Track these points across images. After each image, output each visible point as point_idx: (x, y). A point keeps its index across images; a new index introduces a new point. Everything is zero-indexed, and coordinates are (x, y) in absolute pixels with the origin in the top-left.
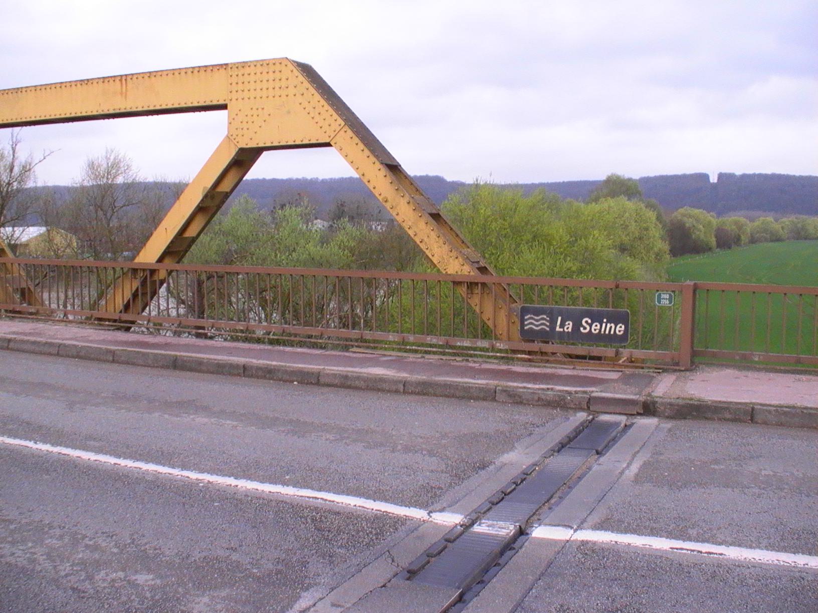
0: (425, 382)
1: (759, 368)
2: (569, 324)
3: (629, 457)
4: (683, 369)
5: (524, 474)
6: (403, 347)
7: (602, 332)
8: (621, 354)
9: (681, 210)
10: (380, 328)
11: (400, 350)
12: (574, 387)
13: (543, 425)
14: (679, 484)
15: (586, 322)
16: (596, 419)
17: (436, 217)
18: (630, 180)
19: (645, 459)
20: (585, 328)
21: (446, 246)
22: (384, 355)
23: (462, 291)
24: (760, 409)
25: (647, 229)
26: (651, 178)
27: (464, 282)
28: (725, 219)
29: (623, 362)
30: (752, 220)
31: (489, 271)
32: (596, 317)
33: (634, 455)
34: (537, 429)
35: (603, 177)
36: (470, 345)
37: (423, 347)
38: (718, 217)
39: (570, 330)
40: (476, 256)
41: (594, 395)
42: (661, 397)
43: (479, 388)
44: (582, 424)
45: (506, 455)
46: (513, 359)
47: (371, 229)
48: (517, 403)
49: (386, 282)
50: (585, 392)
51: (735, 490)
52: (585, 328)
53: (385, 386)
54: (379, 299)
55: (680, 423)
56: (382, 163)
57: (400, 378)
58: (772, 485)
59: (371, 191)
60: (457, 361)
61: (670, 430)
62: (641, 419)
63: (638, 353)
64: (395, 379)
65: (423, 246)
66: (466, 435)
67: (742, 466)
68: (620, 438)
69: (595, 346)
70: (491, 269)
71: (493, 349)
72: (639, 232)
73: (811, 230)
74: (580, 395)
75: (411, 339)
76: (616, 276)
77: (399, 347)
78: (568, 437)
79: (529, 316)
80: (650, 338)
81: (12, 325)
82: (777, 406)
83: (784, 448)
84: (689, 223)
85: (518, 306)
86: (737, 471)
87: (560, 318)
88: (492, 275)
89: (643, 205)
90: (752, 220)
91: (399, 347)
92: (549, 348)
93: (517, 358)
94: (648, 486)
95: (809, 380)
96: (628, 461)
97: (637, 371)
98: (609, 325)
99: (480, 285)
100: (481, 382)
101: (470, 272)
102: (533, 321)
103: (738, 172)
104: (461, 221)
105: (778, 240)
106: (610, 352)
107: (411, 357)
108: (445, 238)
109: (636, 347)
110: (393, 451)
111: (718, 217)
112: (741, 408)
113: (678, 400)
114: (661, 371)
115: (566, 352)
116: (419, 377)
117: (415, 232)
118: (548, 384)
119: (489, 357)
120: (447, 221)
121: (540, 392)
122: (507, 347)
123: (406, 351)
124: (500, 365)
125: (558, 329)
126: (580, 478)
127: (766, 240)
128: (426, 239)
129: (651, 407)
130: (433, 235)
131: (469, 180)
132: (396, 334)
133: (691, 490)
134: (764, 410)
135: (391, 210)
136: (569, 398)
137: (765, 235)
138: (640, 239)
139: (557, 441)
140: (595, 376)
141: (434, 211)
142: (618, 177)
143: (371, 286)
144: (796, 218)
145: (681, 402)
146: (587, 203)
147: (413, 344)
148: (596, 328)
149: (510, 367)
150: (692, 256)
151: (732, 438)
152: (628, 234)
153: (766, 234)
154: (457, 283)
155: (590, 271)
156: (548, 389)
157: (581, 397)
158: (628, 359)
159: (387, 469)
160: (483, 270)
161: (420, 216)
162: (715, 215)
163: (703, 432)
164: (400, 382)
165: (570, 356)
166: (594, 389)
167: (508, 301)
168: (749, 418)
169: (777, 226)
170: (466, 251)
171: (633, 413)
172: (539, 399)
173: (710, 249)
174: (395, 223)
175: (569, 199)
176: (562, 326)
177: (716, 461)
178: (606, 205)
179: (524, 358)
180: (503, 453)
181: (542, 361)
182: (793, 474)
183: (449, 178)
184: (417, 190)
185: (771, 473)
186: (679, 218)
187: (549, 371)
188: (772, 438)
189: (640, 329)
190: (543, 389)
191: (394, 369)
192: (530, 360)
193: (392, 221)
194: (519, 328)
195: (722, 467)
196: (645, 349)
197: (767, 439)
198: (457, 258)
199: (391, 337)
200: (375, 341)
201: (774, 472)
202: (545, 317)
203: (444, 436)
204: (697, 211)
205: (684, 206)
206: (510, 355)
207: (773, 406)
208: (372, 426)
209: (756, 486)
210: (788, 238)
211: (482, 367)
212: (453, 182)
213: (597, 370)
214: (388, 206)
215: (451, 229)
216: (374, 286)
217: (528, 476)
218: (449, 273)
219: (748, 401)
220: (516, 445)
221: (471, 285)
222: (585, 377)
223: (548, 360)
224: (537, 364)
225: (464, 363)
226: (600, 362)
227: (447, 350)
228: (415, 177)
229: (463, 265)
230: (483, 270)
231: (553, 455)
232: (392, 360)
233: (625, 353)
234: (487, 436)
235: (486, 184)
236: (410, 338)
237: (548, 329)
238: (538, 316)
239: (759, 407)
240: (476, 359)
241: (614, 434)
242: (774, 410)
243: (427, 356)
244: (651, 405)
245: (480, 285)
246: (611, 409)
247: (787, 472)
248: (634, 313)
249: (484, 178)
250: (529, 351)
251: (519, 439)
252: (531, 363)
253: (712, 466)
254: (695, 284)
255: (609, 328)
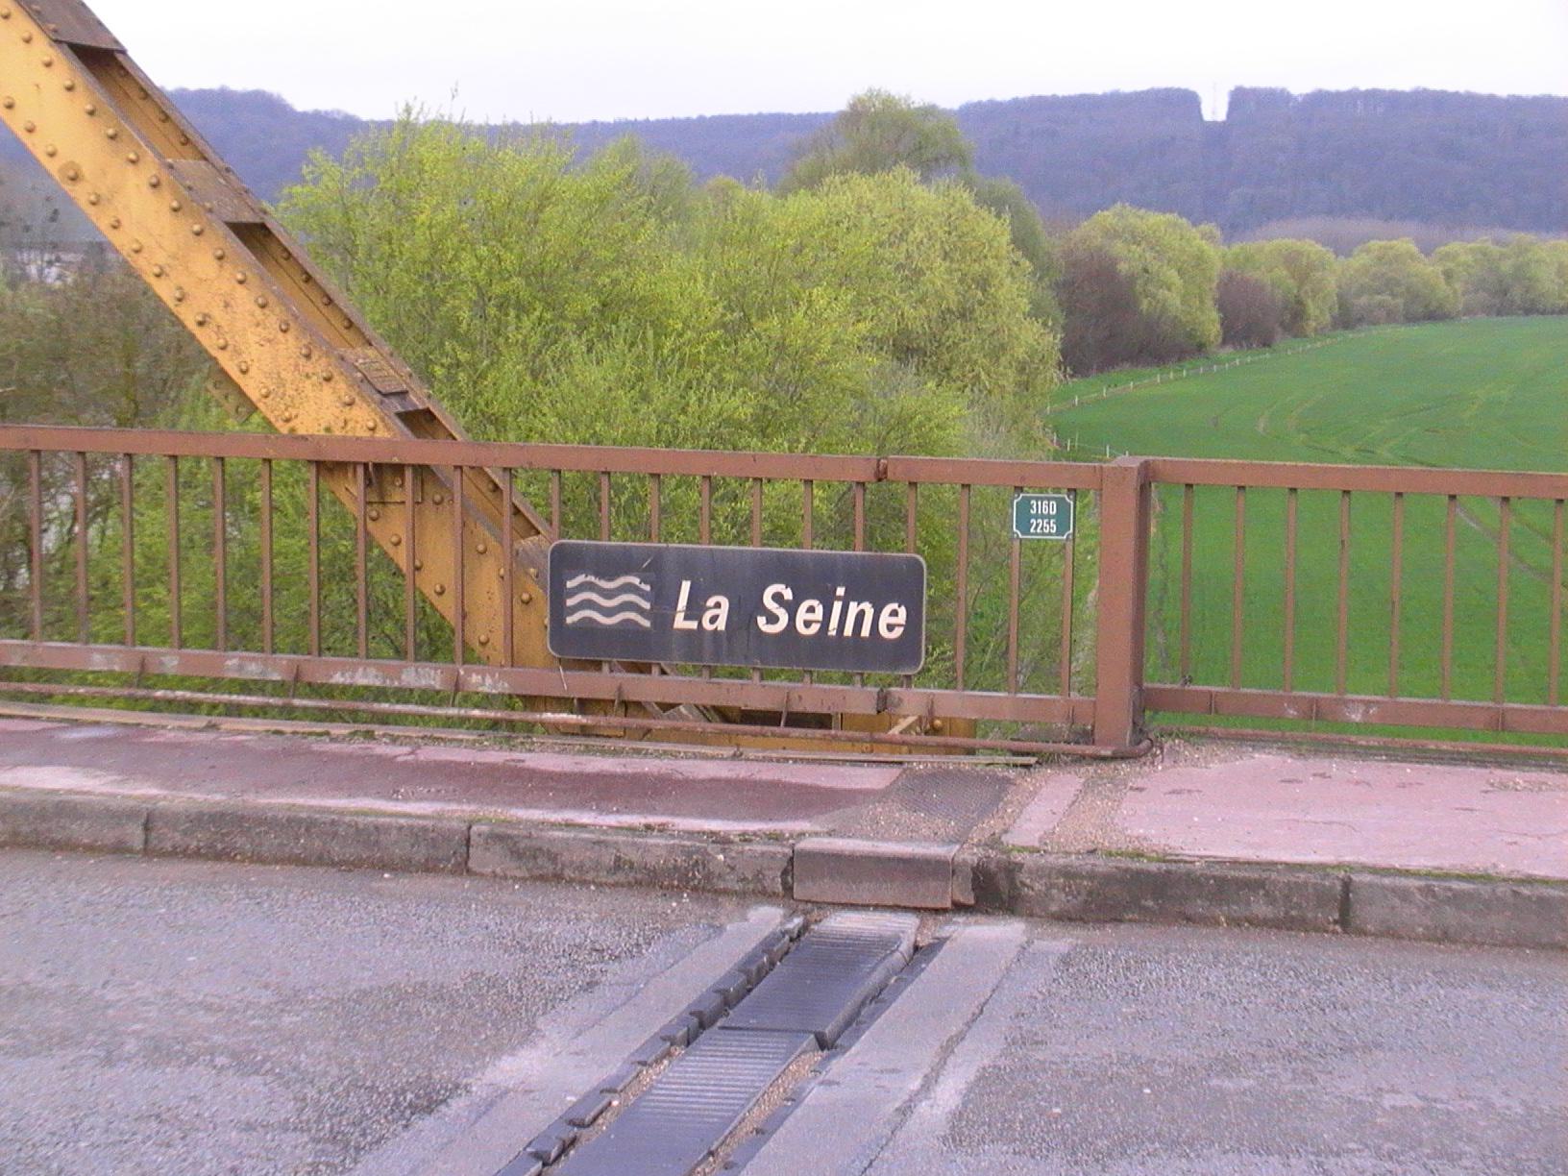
0: (223, 815)
1: (1368, 748)
2: (718, 605)
3: (927, 1057)
4: (1108, 753)
5: (572, 1123)
6: (141, 692)
7: (832, 632)
8: (898, 705)
9: (1107, 217)
10: (57, 627)
11: (133, 703)
12: (737, 819)
13: (634, 951)
14: (1103, 1144)
15: (778, 598)
16: (814, 927)
17: (254, 235)
18: (929, 111)
19: (986, 1062)
20: (773, 619)
21: (290, 336)
22: (76, 723)
23: (351, 491)
24: (1370, 885)
25: (984, 283)
26: (1000, 104)
27: (355, 464)
28: (1251, 246)
29: (904, 732)
30: (1342, 247)
31: (440, 423)
32: (812, 582)
33: (947, 1049)
34: (615, 966)
35: (833, 100)
36: (378, 683)
37: (215, 690)
38: (1228, 240)
39: (721, 624)
40: (396, 374)
41: (807, 844)
42: (1033, 850)
43: (411, 827)
44: (767, 945)
45: (506, 1063)
46: (530, 728)
47: (25, 277)
48: (542, 878)
49: (79, 465)
50: (776, 837)
51: (1293, 1161)
52: (773, 619)
53: (81, 832)
54: (54, 529)
55: (1105, 937)
56: (57, 42)
57: (132, 803)
58: (1421, 1143)
59: (17, 141)
60: (333, 740)
61: (1066, 961)
62: (966, 924)
63: (955, 703)
64: (113, 804)
65: (207, 339)
66: (365, 993)
67: (1314, 1081)
68: (898, 991)
69: (807, 678)
70: (442, 410)
71: (457, 692)
72: (957, 293)
73: (1547, 280)
74: (759, 848)
75: (171, 662)
76: (881, 443)
77: (126, 692)
78: (717, 991)
79: (581, 579)
80: (995, 649)
81: (895, 919)
82: (1428, 875)
83: (1457, 1016)
84: (1128, 259)
85: (541, 545)
86: (1300, 1096)
87: (686, 586)
88: (454, 438)
89: (966, 198)
90: (1342, 247)
91: (126, 692)
92: (647, 687)
93: (543, 723)
94: (995, 1153)
95: (1540, 786)
96: (927, 1070)
97: (951, 762)
98: (854, 608)
99: (409, 474)
100: (419, 808)
101: (373, 429)
102: (594, 597)
103: (1300, 86)
104: (350, 251)
105: (1430, 313)
106: (858, 699)
107: (172, 727)
108: (288, 309)
109: (951, 684)
110: (109, 1061)
111: (1228, 240)
112: (1306, 884)
113: (1091, 860)
114: (1032, 760)
115: (709, 702)
116: (199, 796)
117: (180, 288)
118: (653, 811)
119: (449, 723)
120: (294, 250)
121: (621, 838)
122: (504, 687)
123: (157, 706)
124: (484, 749)
125: (680, 622)
126: (762, 1133)
127: (1391, 317)
128: (218, 313)
129: (1003, 884)
130: (245, 300)
131: (374, 106)
132: (122, 648)
133: (1143, 1164)
134: (1384, 887)
135: (91, 211)
136: (721, 857)
137: (1386, 298)
138: (964, 314)
139: (684, 1006)
140: (808, 781)
141: (247, 217)
142: (889, 103)
143: (26, 483)
144: (1497, 242)
145: (1102, 864)
146: (784, 193)
147: (182, 682)
148: (810, 617)
149: (516, 755)
150: (1140, 370)
151: (1277, 985)
152: (921, 301)
153: (1394, 295)
154: (328, 468)
155: (793, 421)
156: (648, 827)
157: (763, 854)
158: (920, 719)
159: (86, 1124)
160: (420, 421)
161: (198, 234)
162: (1218, 233)
163: (1180, 966)
164: (131, 814)
165: (724, 714)
166: (803, 825)
167: (507, 528)
168: (1336, 916)
169: (1428, 270)
170: (362, 355)
171: (939, 905)
172: (618, 865)
173: (1200, 348)
174: (111, 256)
175: (721, 179)
176: (695, 610)
177: (1229, 1066)
178: (844, 200)
179: (566, 724)
180: (498, 1051)
181: (626, 733)
182: (1489, 1105)
183: (303, 100)
184: (187, 142)
185: (1416, 1103)
186: (1099, 241)
187: (650, 766)
188: (1418, 983)
189: (961, 627)
190: (632, 829)
191: (107, 769)
192: (584, 731)
193: (100, 248)
194: (547, 621)
195: (1246, 1083)
196: (982, 689)
197: (1397, 989)
198: (328, 380)
199: (100, 658)
200: (41, 674)
201: (1424, 1098)
202: (636, 581)
203: (291, 999)
204: (1155, 220)
205: (1115, 202)
206: (516, 716)
207: (1416, 875)
208: (31, 975)
209: (1367, 1146)
210: (1469, 311)
211: (422, 758)
212: (318, 116)
213: (814, 761)
214: (81, 194)
215: (309, 279)
216: (34, 481)
217: (584, 1131)
218: (301, 431)
219: (1328, 858)
220: (540, 1022)
221: (380, 474)
222: (775, 785)
223: (649, 731)
224: (609, 744)
225: (357, 746)
226: (826, 732)
227: (297, 702)
228: (182, 93)
229: (350, 404)
230: (420, 421)
231: (668, 1054)
232: (99, 741)
233: (912, 702)
234: (440, 995)
235: (439, 126)
236: (165, 659)
237: (646, 623)
238: (611, 579)
239: (1367, 878)
240: (396, 731)
241: (877, 977)
242: (1419, 889)
243: (229, 724)
244: (1001, 875)
245: (409, 474)
246: (864, 892)
247: (1468, 1098)
248: (942, 567)
249: (434, 104)
250: (580, 700)
251: (550, 1003)
252: (591, 742)
253: (1214, 1082)
254: (1146, 465)
255: (854, 616)
